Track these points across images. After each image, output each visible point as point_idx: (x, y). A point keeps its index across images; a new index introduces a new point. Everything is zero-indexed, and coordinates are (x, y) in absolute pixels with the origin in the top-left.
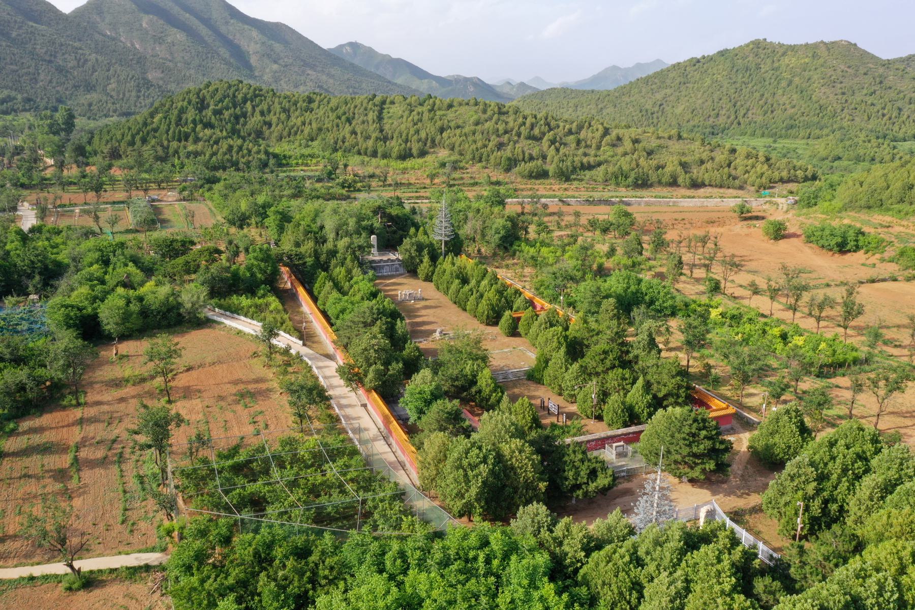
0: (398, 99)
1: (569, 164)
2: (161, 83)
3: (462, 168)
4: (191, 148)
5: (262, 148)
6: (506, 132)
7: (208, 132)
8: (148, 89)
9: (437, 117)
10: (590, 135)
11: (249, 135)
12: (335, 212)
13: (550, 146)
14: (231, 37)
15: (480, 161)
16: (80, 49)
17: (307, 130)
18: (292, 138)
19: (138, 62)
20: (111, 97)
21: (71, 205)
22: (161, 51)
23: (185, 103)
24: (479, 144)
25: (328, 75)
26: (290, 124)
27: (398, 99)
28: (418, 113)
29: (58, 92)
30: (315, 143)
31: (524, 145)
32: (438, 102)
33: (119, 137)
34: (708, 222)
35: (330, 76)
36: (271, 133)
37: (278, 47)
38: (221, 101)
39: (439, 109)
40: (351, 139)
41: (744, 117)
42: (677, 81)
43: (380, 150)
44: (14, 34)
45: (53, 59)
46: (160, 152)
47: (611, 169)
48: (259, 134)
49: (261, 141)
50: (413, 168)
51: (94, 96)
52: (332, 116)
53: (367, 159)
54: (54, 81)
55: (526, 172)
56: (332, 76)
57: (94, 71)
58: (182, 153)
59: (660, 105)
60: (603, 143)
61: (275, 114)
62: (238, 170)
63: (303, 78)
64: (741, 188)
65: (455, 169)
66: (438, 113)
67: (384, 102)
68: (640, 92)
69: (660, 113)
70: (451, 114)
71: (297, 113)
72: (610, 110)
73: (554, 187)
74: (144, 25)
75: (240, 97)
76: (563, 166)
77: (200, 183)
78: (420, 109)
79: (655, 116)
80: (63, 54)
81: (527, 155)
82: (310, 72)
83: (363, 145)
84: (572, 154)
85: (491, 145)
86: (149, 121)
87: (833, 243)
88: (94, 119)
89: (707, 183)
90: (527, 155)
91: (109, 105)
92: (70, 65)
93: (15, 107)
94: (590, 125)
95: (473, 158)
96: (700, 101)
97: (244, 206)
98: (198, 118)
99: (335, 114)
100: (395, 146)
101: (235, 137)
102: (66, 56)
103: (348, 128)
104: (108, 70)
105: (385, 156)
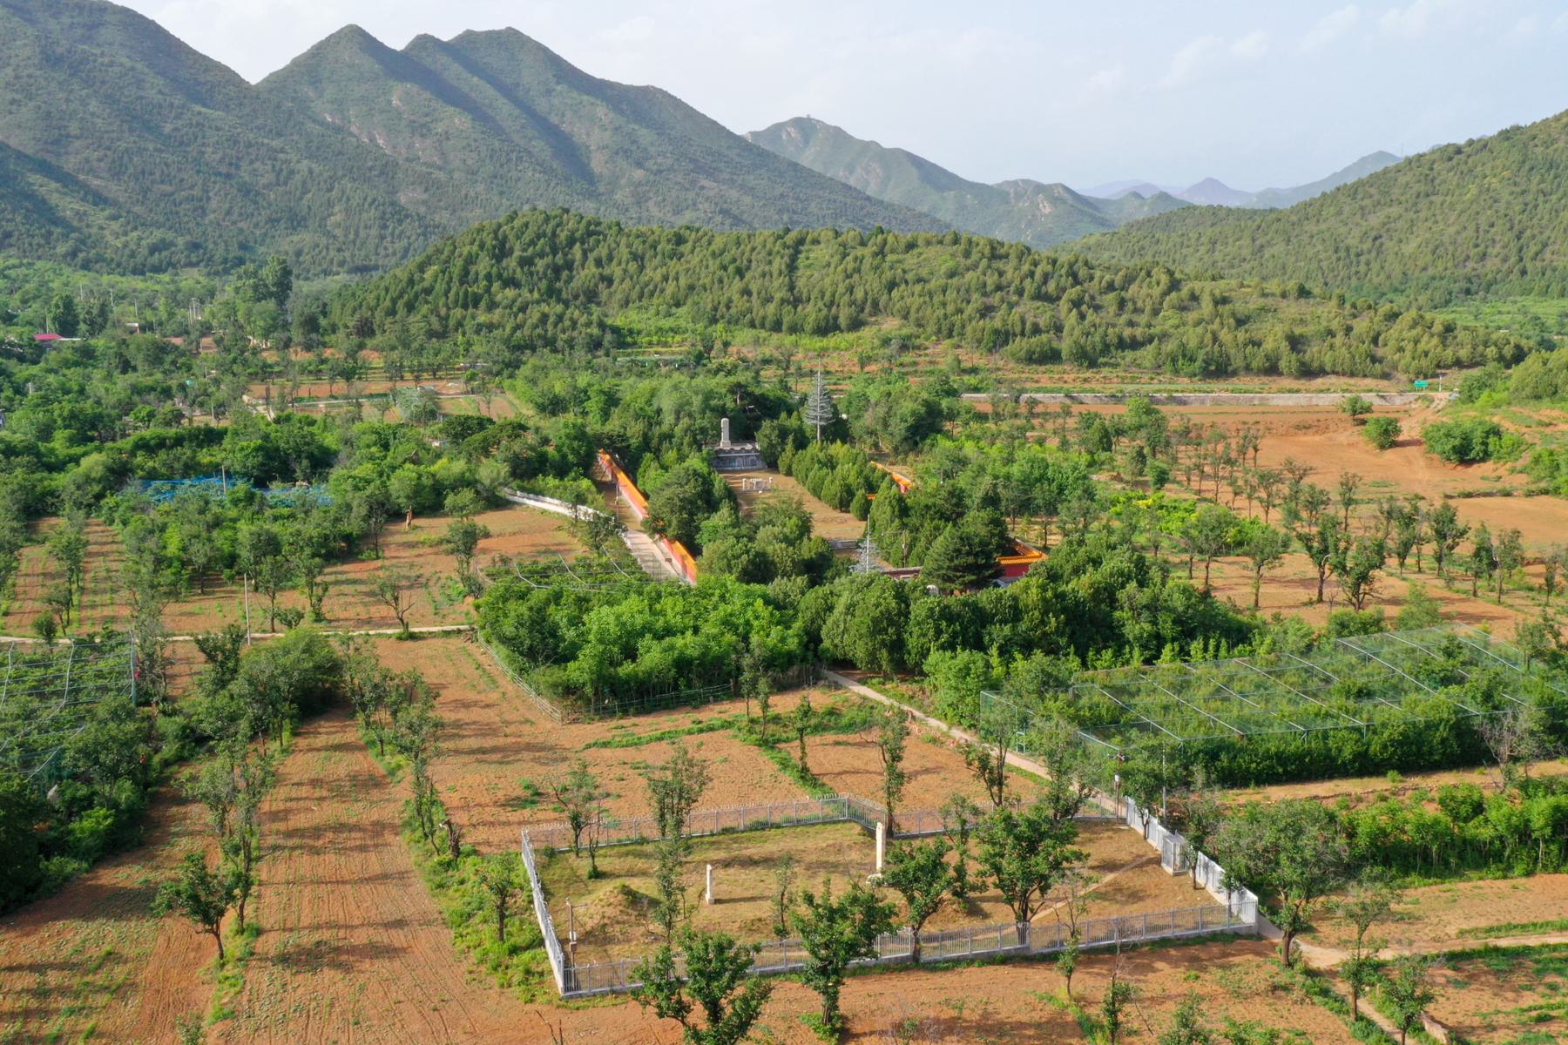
0: (825, 235)
1: (1097, 339)
2: (422, 210)
3: (919, 348)
4: (483, 318)
5: (594, 317)
6: (999, 288)
7: (510, 293)
8: (400, 222)
9: (886, 265)
10: (1144, 291)
11: (576, 297)
12: (676, 387)
13: (1070, 311)
14: (554, 119)
15: (950, 336)
16: (282, 151)
17: (670, 288)
18: (645, 302)
19: (382, 173)
20: (335, 237)
21: (310, 398)
22: (424, 149)
23: (475, 248)
24: (950, 308)
25: (742, 187)
26: (644, 278)
27: (825, 235)
28: (856, 259)
29: (241, 231)
30: (682, 310)
31: (1029, 310)
32: (890, 239)
33: (373, 303)
34: (1298, 427)
35: (746, 189)
36: (611, 295)
37: (645, 135)
38: (532, 243)
39: (893, 251)
40: (739, 303)
41: (1534, 259)
42: (1413, 191)
43: (786, 320)
44: (168, 128)
45: (233, 171)
46: (436, 325)
47: (1170, 346)
48: (591, 296)
49: (593, 307)
50: (836, 348)
51: (304, 238)
52: (713, 265)
53: (763, 334)
54: (236, 210)
55: (1022, 354)
56: (751, 191)
57: (305, 191)
58: (469, 325)
59: (1375, 239)
60: (1165, 305)
61: (620, 264)
62: (555, 351)
63: (691, 195)
64: (1386, 376)
65: (904, 348)
66: (890, 258)
67: (801, 241)
68: (1340, 213)
69: (1374, 254)
70: (910, 260)
71: (656, 261)
72: (1279, 248)
73: (1066, 377)
74: (395, 102)
75: (563, 236)
76: (1088, 343)
77: (495, 369)
78: (860, 251)
79: (1363, 259)
80: (252, 162)
81: (1028, 326)
82: (705, 183)
83: (758, 312)
84: (1109, 321)
85: (970, 310)
86: (416, 277)
87: (1448, 447)
88: (307, 279)
89: (1328, 368)
90: (1028, 326)
91: (332, 253)
92: (263, 181)
93: (174, 260)
94: (1149, 274)
95: (939, 331)
96: (1452, 230)
97: (559, 388)
98: (495, 270)
99: (718, 261)
100: (811, 313)
101: (553, 301)
102: (257, 165)
103: (737, 284)
104: (330, 190)
105: (794, 329)
